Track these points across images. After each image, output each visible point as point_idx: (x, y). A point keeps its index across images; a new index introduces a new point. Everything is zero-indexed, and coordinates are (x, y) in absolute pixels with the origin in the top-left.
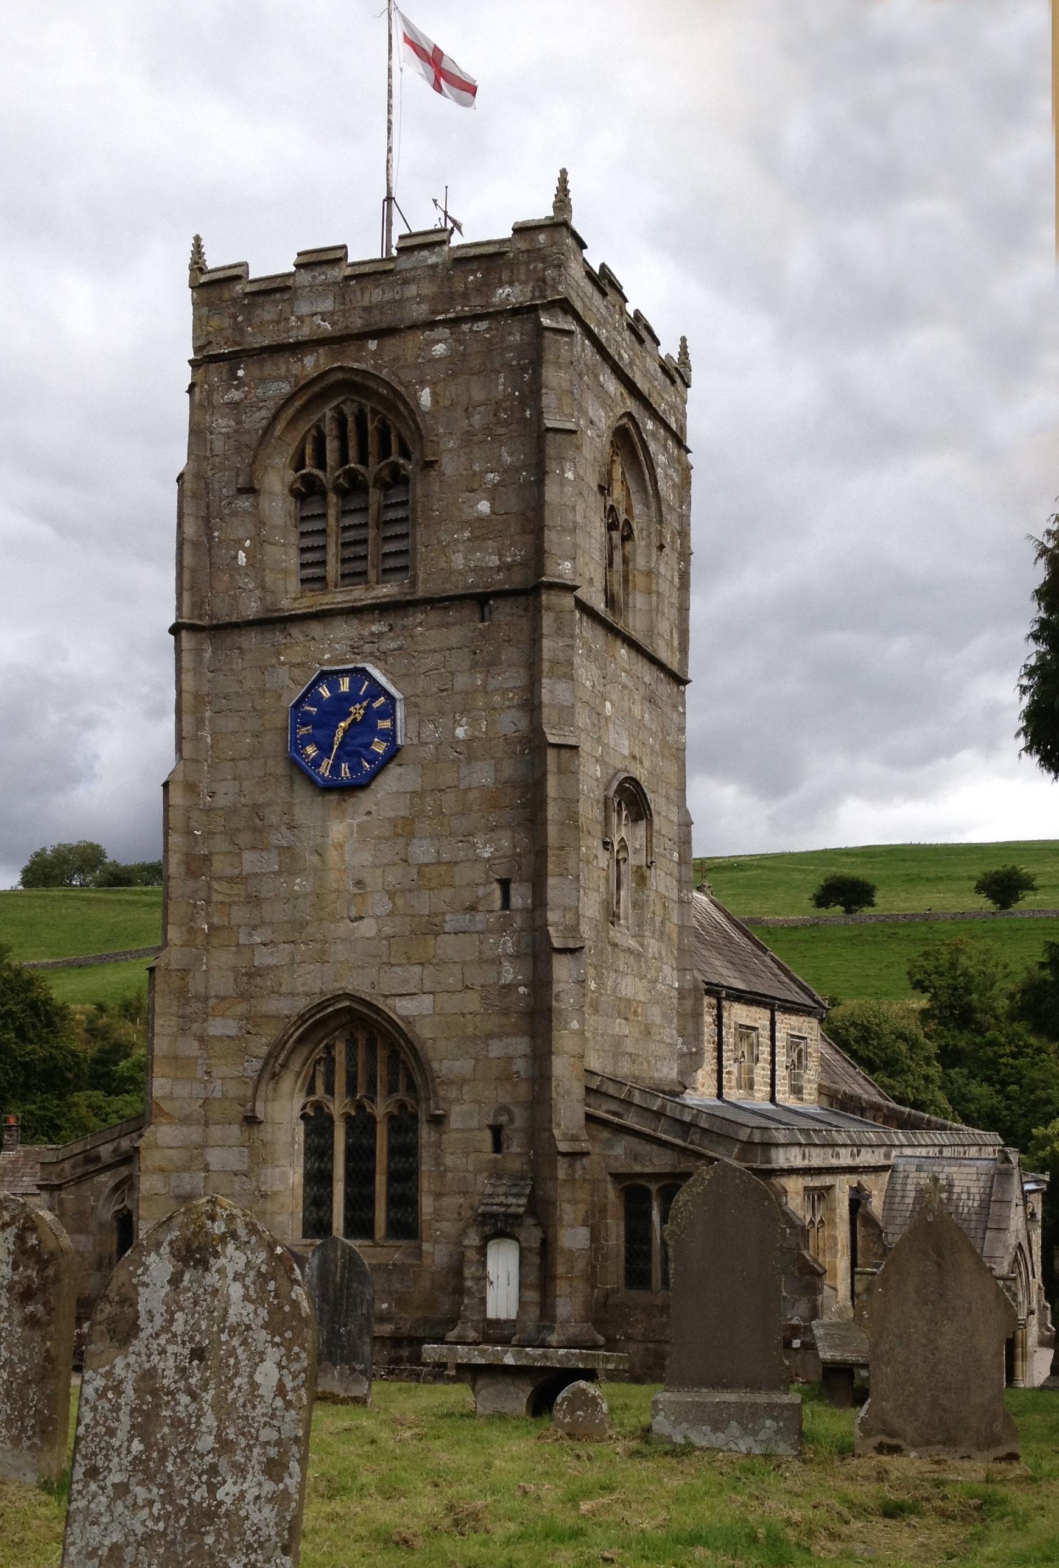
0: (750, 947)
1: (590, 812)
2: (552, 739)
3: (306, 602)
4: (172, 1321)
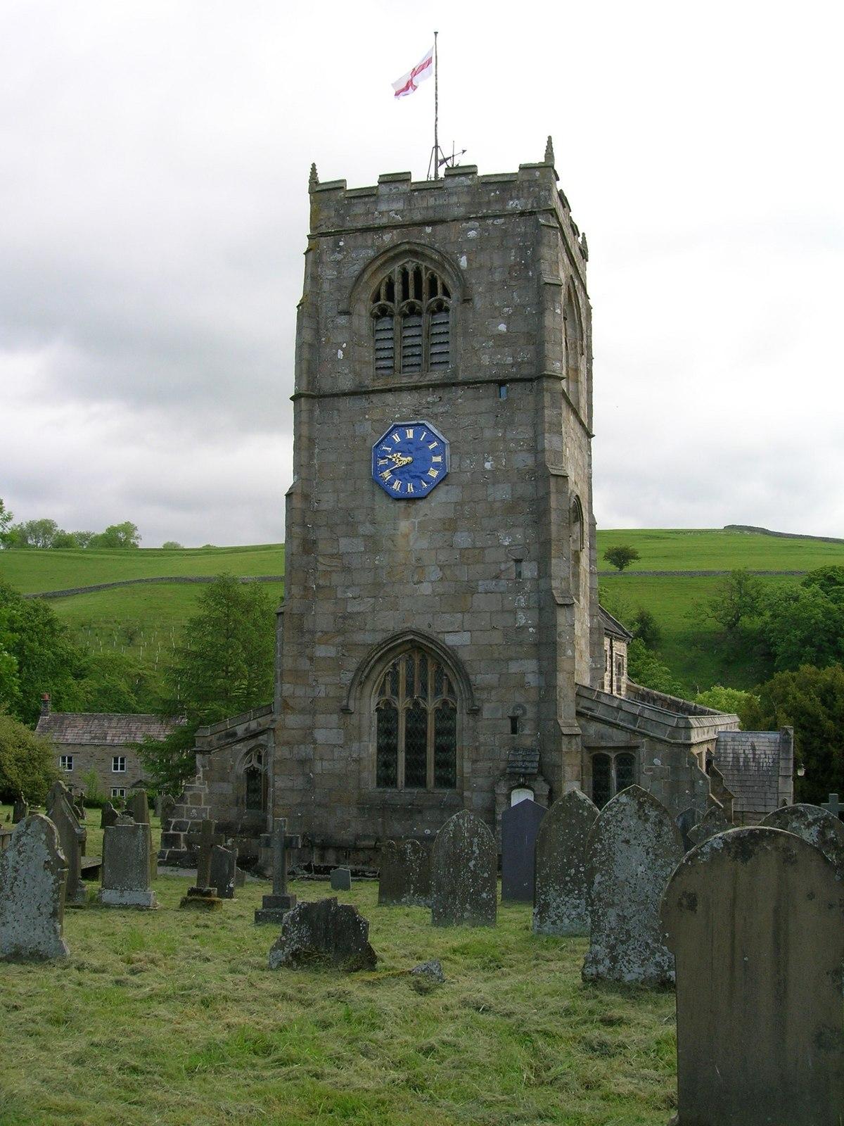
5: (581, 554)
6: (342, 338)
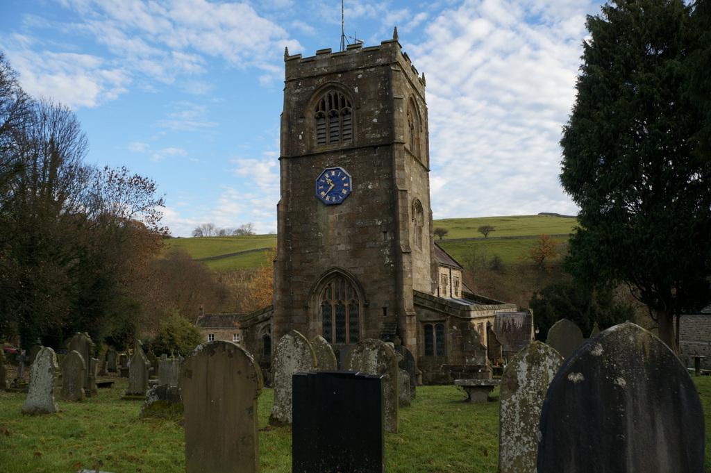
2: (399, 188)
4: (529, 383)
5: (423, 228)
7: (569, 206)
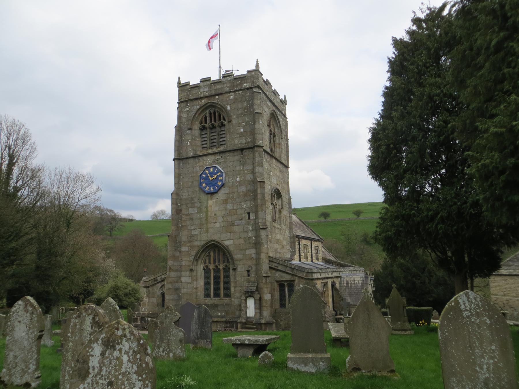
0: (305, 227)
1: (268, 197)
3: (203, 152)
4: (101, 370)
6: (189, 138)
7: (373, 193)
